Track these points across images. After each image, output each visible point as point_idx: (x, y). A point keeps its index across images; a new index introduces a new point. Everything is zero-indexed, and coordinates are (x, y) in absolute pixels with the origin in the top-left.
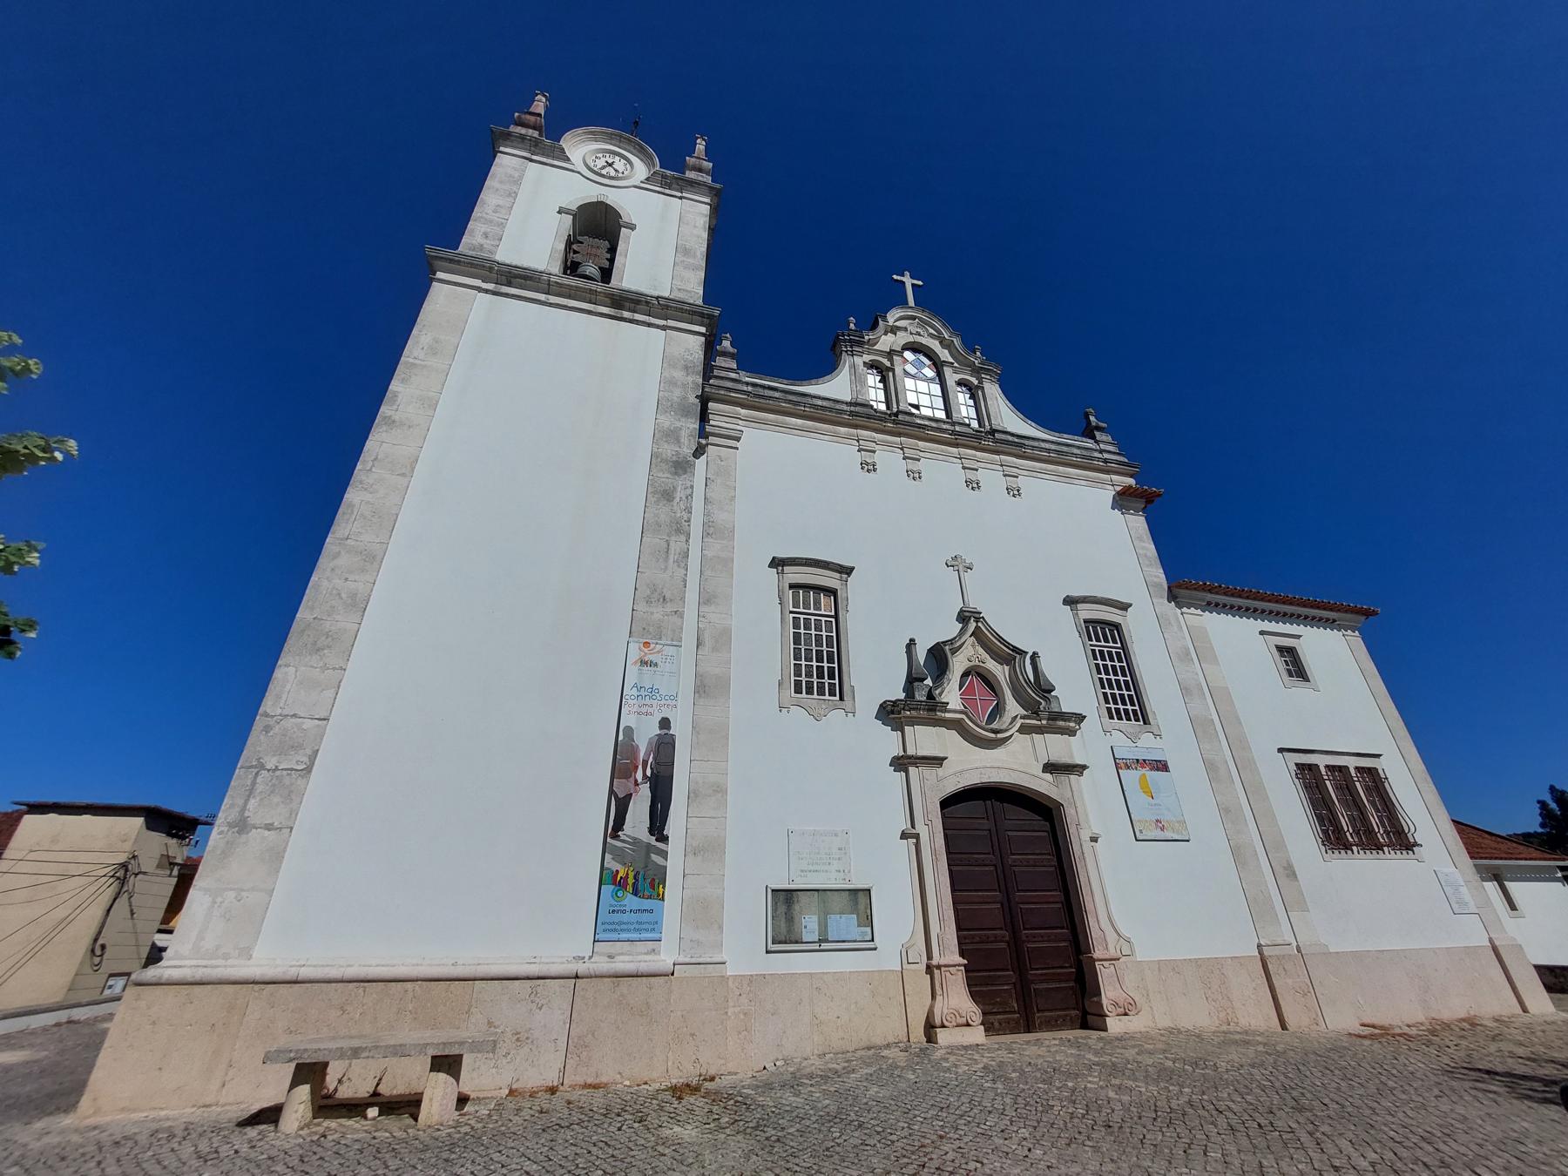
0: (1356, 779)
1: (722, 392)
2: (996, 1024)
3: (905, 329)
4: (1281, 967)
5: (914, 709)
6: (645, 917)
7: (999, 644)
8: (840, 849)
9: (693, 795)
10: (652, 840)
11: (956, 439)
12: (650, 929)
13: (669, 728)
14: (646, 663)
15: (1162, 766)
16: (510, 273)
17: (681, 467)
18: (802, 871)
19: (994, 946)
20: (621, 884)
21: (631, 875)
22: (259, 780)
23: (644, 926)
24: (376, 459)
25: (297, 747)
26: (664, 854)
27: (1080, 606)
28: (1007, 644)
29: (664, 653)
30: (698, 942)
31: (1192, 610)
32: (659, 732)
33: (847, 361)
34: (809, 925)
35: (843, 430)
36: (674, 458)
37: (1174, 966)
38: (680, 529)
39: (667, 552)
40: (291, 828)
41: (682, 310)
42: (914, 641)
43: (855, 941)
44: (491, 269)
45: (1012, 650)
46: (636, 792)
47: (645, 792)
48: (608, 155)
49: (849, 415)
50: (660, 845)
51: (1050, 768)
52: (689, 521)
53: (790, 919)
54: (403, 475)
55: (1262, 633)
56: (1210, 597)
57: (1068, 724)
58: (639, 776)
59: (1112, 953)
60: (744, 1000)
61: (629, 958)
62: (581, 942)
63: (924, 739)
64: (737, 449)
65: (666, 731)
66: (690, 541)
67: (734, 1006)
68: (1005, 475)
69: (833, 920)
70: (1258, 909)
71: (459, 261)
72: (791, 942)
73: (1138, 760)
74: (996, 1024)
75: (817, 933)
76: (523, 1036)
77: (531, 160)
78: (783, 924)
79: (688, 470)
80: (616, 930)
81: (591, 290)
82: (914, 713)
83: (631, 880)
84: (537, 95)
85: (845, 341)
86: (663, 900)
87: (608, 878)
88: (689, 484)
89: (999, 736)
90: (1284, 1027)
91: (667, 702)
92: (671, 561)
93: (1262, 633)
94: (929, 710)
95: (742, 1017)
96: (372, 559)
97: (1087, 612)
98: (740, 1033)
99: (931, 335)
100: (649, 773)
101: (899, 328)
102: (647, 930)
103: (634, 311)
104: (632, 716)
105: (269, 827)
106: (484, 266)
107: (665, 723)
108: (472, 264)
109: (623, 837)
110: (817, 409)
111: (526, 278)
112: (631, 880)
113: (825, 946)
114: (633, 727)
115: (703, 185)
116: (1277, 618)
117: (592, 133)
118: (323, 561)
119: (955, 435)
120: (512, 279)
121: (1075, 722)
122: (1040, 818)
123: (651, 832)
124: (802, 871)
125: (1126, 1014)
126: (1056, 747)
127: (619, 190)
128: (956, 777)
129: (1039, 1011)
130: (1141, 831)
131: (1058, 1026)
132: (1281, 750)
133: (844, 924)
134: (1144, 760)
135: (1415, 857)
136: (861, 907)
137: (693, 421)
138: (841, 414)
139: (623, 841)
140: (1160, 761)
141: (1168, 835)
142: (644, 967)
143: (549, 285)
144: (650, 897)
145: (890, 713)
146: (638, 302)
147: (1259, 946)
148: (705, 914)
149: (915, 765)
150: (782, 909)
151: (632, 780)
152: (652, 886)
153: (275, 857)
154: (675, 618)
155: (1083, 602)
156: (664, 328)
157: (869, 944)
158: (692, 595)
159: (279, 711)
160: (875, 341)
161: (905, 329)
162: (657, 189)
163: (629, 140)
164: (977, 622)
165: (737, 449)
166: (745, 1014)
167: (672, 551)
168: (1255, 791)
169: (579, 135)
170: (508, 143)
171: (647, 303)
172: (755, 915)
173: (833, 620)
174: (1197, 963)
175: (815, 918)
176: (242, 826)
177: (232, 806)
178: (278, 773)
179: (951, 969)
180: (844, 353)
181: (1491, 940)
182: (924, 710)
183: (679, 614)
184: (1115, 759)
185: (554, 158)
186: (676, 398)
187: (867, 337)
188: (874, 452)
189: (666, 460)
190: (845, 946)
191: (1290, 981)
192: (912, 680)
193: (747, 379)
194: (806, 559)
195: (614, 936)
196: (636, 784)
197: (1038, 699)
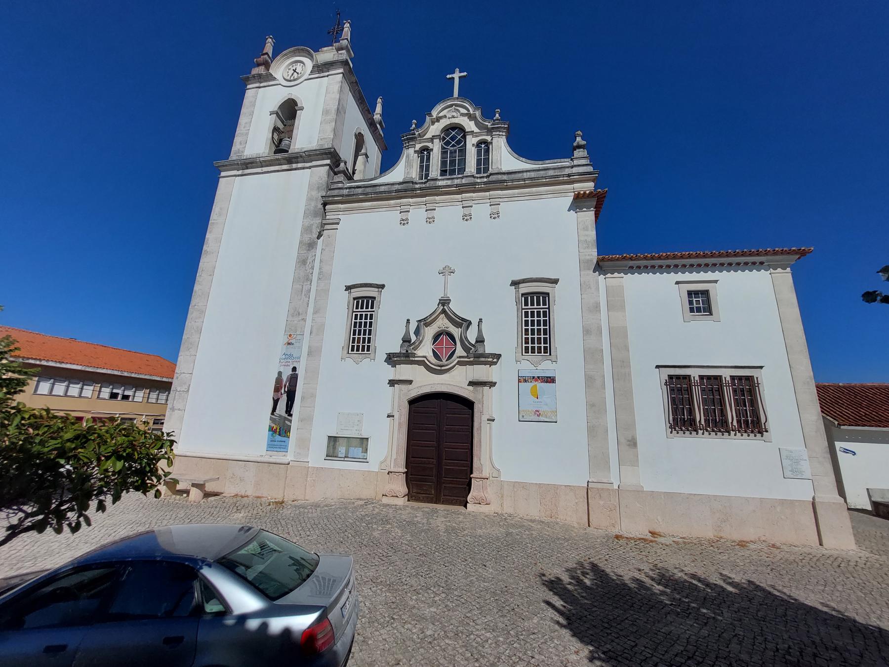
0: (756, 385)
1: (331, 199)
2: (421, 498)
3: (445, 116)
4: (598, 495)
5: (398, 357)
6: (283, 443)
7: (454, 317)
8: (359, 421)
9: (303, 398)
10: (286, 416)
11: (459, 189)
12: (284, 448)
13: (296, 371)
14: (289, 344)
15: (551, 380)
17: (311, 245)
18: (342, 429)
19: (428, 466)
20: (275, 431)
21: (278, 428)
22: (176, 395)
23: (282, 447)
24: (203, 270)
25: (185, 384)
26: (290, 421)
27: (521, 285)
28: (459, 317)
29: (297, 338)
30: (300, 454)
31: (616, 275)
32: (291, 373)
33: (406, 152)
34: (342, 451)
35: (392, 202)
36: (309, 242)
37: (524, 486)
38: (308, 279)
39: (302, 291)
40: (185, 410)
41: (317, 155)
42: (409, 320)
43: (360, 459)
45: (462, 320)
46: (281, 397)
47: (285, 397)
48: (294, 64)
49: (395, 193)
50: (289, 418)
51: (471, 383)
52: (312, 273)
53: (334, 448)
54: (210, 275)
55: (677, 283)
56: (631, 263)
57: (487, 359)
58: (283, 391)
59: (485, 474)
60: (314, 475)
61: (278, 457)
62: (264, 452)
63: (404, 371)
64: (337, 229)
65: (294, 372)
66: (312, 283)
67: (310, 477)
68: (463, 207)
69: (351, 449)
70: (598, 460)
71: (226, 165)
72: (334, 457)
73: (534, 377)
74: (421, 498)
75: (344, 454)
76: (242, 479)
77: (259, 87)
78: (331, 450)
79: (314, 247)
80: (272, 447)
81: (277, 159)
82: (398, 359)
83: (278, 430)
84: (267, 39)
85: (404, 140)
86: (289, 438)
87: (271, 429)
88: (314, 254)
89: (443, 368)
91: (296, 360)
92: (303, 295)
93: (677, 283)
94: (405, 357)
95: (313, 481)
96: (202, 312)
97: (525, 288)
98: (311, 487)
99: (463, 115)
100: (286, 390)
101: (441, 118)
102: (283, 448)
103: (297, 163)
104: (282, 367)
105: (179, 410)
106: (235, 164)
107: (294, 369)
108: (230, 164)
109: (275, 414)
110: (378, 194)
111: (252, 163)
112: (278, 430)
113: (346, 459)
114: (281, 371)
115: (338, 62)
116: (707, 268)
117: (285, 55)
118: (189, 316)
119: (459, 187)
120: (248, 164)
121: (492, 358)
122: (465, 408)
123: (286, 413)
124: (342, 429)
125: (480, 504)
126: (480, 372)
127: (298, 86)
128: (415, 391)
129: (444, 496)
130: (523, 416)
131: (452, 503)
132: (657, 367)
133: (357, 452)
134: (538, 377)
135: (763, 438)
136: (364, 445)
137: (319, 218)
138: (391, 193)
139: (276, 416)
140: (550, 377)
141: (541, 419)
142: (278, 461)
143: (261, 163)
144: (284, 437)
145: (392, 359)
146: (297, 157)
148: (304, 444)
149: (397, 383)
150: (332, 444)
151: (280, 393)
152: (285, 432)
153: (181, 419)
154: (302, 322)
155: (523, 283)
156: (310, 168)
157: (365, 460)
158: (311, 310)
159: (180, 372)
160: (424, 133)
161: (445, 116)
162: (317, 75)
163: (303, 50)
164: (444, 306)
165: (337, 229)
166: (314, 481)
167: (304, 290)
168: (624, 395)
169: (279, 60)
170: (250, 82)
171: (301, 156)
172: (322, 445)
173: (547, 310)
174: (540, 485)
175: (344, 448)
176: (173, 409)
178: (181, 392)
179: (396, 473)
180: (404, 148)
181: (814, 498)
182: (403, 357)
183: (304, 320)
184: (519, 377)
185: (269, 81)
186: (312, 208)
187: (417, 133)
188: (409, 211)
189: (306, 244)
190: (355, 459)
191: (602, 503)
192: (406, 340)
193: (348, 185)
194: (361, 284)
195: (272, 449)
196: (282, 394)
197: (470, 346)
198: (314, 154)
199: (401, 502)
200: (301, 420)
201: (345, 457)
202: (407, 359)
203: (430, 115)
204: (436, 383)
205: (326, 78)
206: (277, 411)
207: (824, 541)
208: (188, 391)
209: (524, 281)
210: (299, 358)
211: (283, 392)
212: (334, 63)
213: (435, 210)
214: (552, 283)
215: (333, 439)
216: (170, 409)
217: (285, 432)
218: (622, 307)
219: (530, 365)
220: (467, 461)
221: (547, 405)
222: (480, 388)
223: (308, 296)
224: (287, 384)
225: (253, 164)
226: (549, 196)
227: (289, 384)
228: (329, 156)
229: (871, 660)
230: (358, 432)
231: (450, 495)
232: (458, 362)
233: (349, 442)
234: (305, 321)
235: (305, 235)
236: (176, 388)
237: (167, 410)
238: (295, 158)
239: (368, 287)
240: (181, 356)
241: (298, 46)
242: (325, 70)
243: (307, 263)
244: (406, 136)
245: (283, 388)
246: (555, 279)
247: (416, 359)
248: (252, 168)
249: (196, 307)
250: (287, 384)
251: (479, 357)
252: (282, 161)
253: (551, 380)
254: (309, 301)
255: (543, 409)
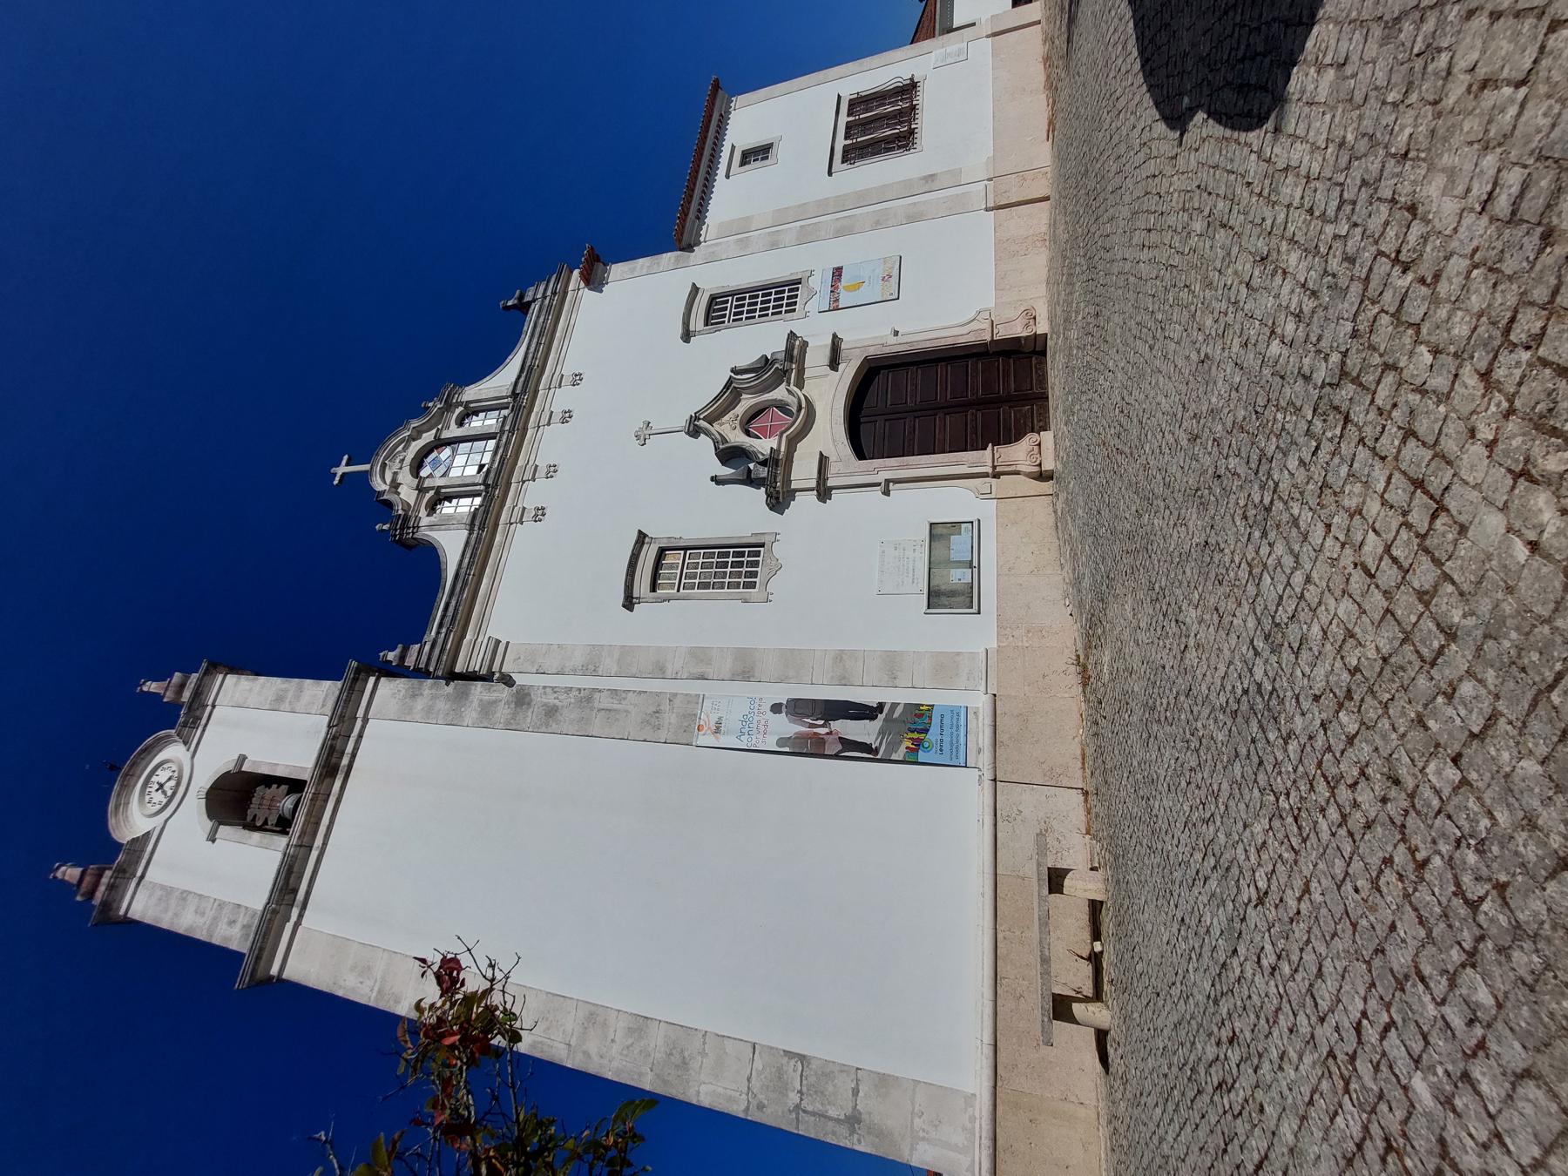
2: (1041, 424)
3: (395, 474)
6: (947, 721)
9: (844, 681)
10: (881, 717)
12: (957, 715)
13: (781, 704)
16: (282, 889)
20: (918, 743)
22: (810, 1108)
25: (780, 1073)
26: (894, 706)
27: (692, 328)
33: (425, 533)
34: (958, 576)
35: (498, 538)
38: (587, 699)
39: (610, 710)
40: (857, 1069)
41: (348, 701)
44: (275, 912)
52: (580, 689)
53: (952, 594)
55: (728, 176)
59: (987, 325)
63: (803, 471)
69: (954, 556)
70: (958, 208)
74: (1041, 424)
83: (915, 735)
85: (401, 534)
87: (911, 760)
89: (803, 405)
90: (1047, 199)
92: (619, 706)
93: (728, 176)
94: (777, 466)
96: (594, 1016)
97: (642, 585)
99: (405, 449)
100: (821, 722)
101: (394, 480)
107: (776, 708)
109: (877, 744)
111: (290, 872)
112: (915, 735)
113: (975, 563)
117: (117, 807)
123: (873, 718)
125: (1035, 318)
126: (816, 358)
132: (830, 173)
133: (959, 546)
136: (945, 531)
139: (881, 744)
142: (988, 720)
143: (301, 846)
144: (930, 718)
145: (779, 501)
146: (332, 749)
147: (987, 210)
148: (946, 667)
150: (944, 600)
152: (921, 716)
154: (677, 701)
155: (688, 326)
161: (395, 474)
170: (115, 905)
171: (335, 738)
173: (688, 552)
175: (953, 571)
177: (834, 1133)
181: (988, 36)
182: (776, 470)
185: (143, 851)
187: (400, 512)
191: (1014, 189)
194: (627, 575)
195: (962, 748)
196: (830, 733)
198: (343, 707)
199: (1047, 437)
200: (893, 682)
201: (971, 566)
202: (781, 463)
203: (383, 493)
204: (829, 417)
205: (215, 711)
206: (870, 739)
207: (1036, 19)
208: (802, 1058)
209: (686, 323)
210: (753, 700)
211: (827, 730)
212: (198, 689)
213: (537, 466)
214: (697, 292)
215: (933, 600)
216: (853, 1132)
217: (921, 716)
218: (748, 219)
219: (813, 300)
220: (967, 366)
221: (874, 270)
222: (843, 354)
223: (624, 695)
224: (809, 720)
225: (295, 869)
226: (574, 316)
227: (808, 717)
228: (362, 675)
229: (1537, 403)
230: (918, 548)
231: (1029, 380)
232: (796, 385)
233: (940, 563)
234: (675, 695)
235: (496, 715)
236: (790, 1111)
237: (857, 1148)
238: (330, 755)
239: (636, 563)
240: (698, 1093)
241: (128, 759)
242: (198, 713)
243: (555, 705)
244: (396, 530)
245: (815, 730)
246: (639, 537)
247: (783, 449)
248: (300, 877)
249: (573, 1043)
250: (809, 720)
251: (792, 356)
252: (323, 789)
253: (838, 272)
254: (634, 691)
255: (880, 273)
